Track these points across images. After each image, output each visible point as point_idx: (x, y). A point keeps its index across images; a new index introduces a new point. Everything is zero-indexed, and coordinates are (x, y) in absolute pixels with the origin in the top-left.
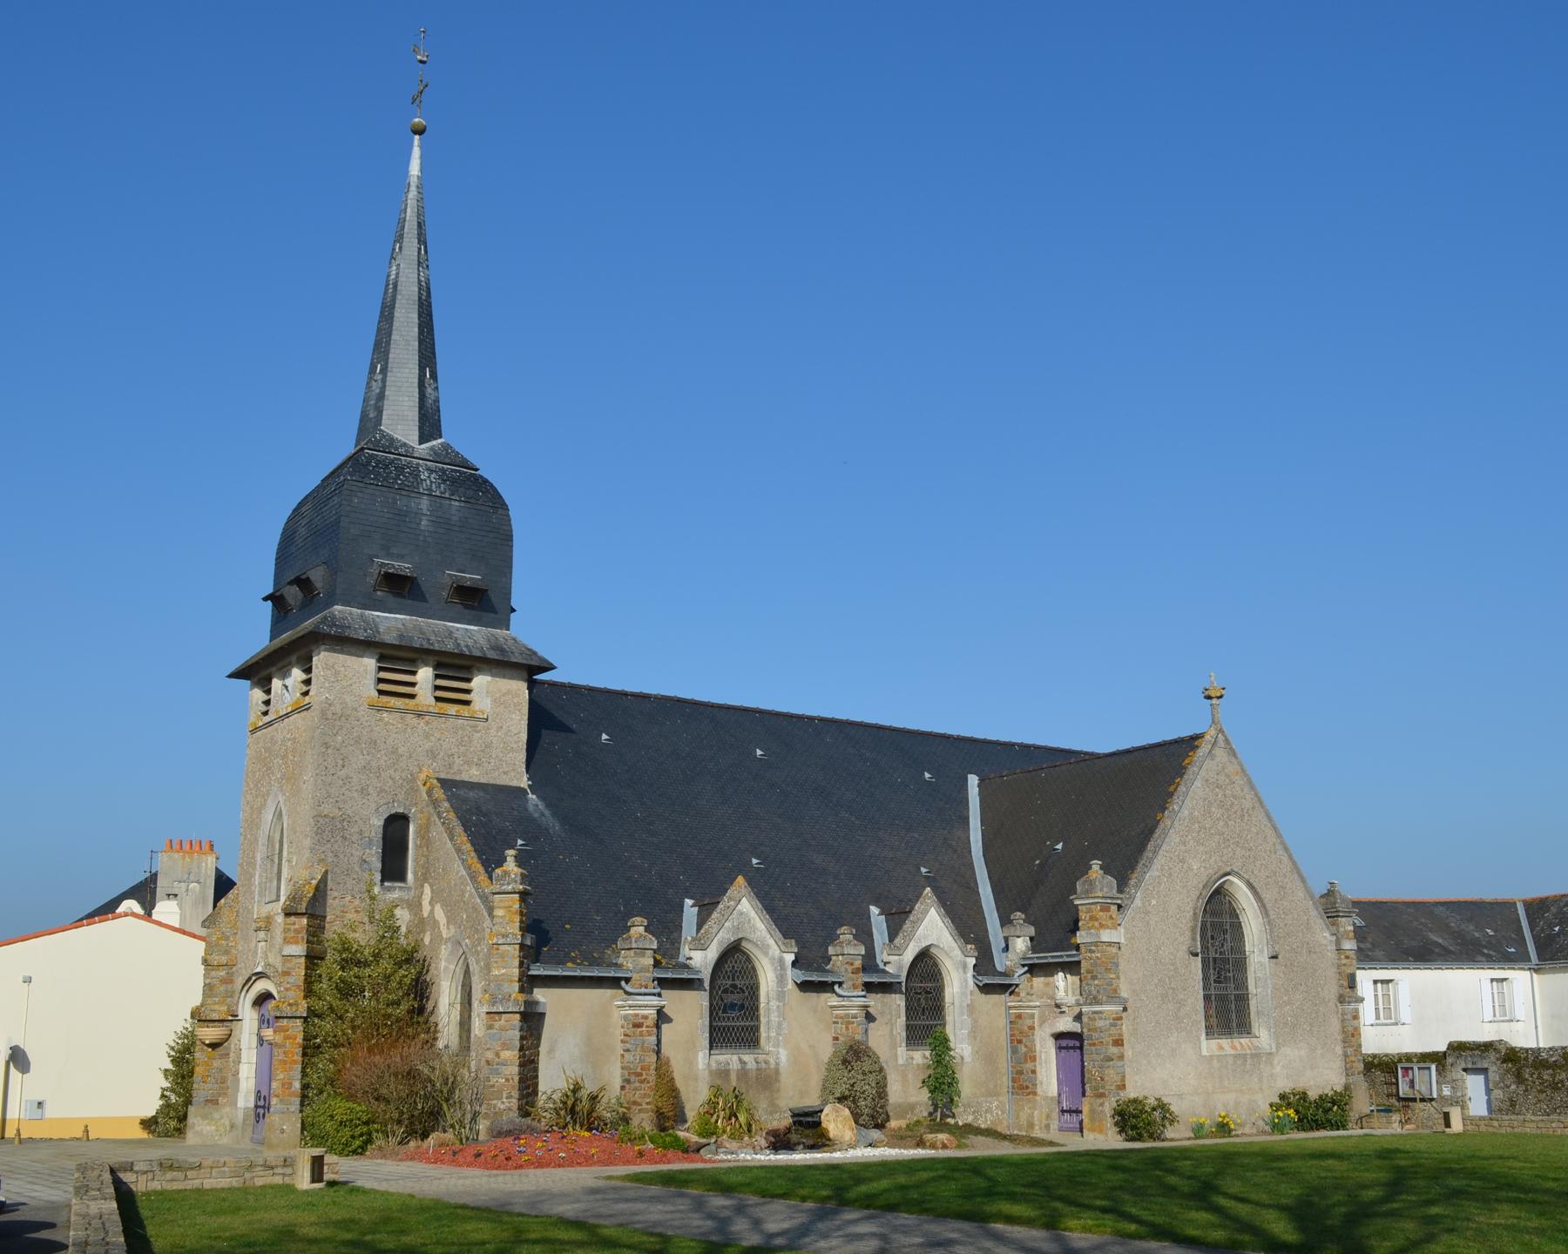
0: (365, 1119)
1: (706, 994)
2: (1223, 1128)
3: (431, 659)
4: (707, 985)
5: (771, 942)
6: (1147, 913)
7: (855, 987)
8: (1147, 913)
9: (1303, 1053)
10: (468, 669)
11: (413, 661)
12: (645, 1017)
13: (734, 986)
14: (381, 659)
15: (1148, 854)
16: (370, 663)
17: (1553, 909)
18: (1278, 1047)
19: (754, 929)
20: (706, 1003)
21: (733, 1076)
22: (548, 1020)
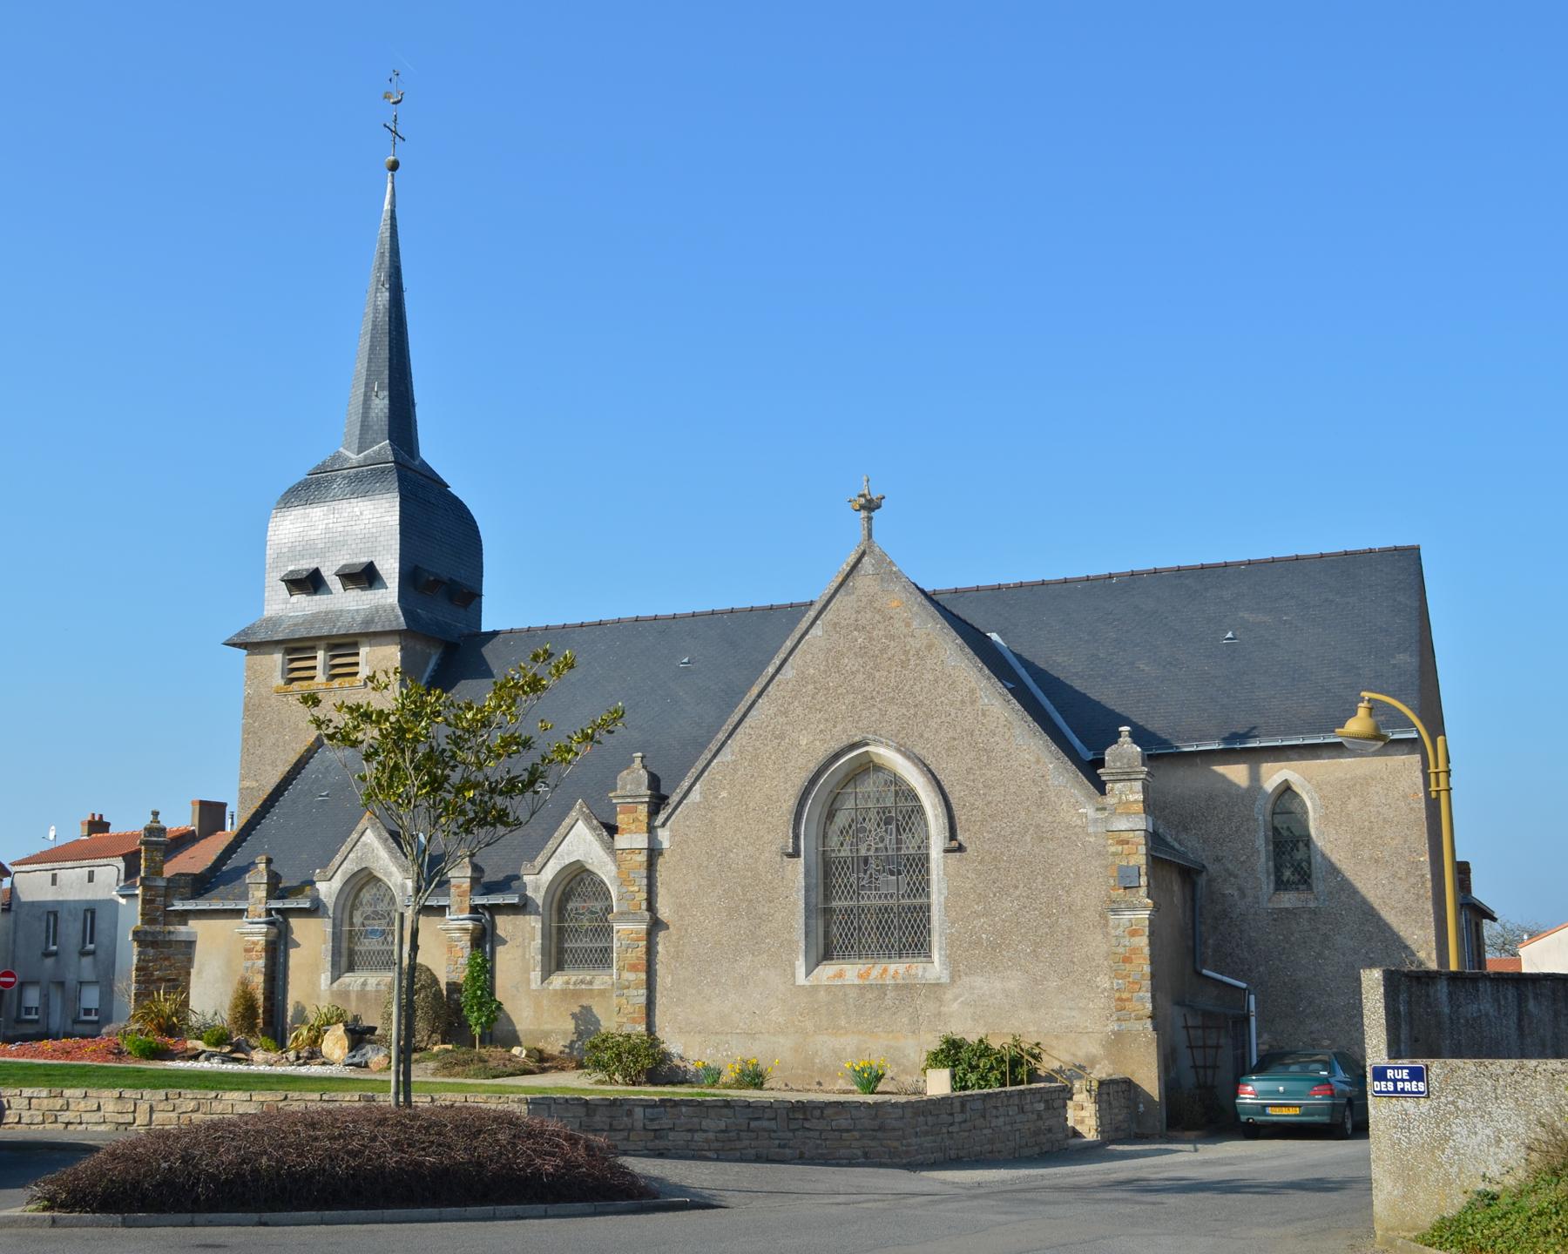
0: (953, 1153)
1: (329, 922)
2: (871, 1080)
3: (323, 643)
4: (330, 913)
5: (394, 869)
6: (712, 808)
7: (461, 911)
8: (712, 808)
9: (1012, 985)
10: (356, 645)
11: (313, 648)
12: (255, 943)
13: (376, 913)
14: (288, 651)
15: (1054, 747)
16: (278, 658)
17: (392, 718)
18: (953, 978)
19: (378, 858)
20: (330, 930)
21: (353, 997)
22: (199, 947)
